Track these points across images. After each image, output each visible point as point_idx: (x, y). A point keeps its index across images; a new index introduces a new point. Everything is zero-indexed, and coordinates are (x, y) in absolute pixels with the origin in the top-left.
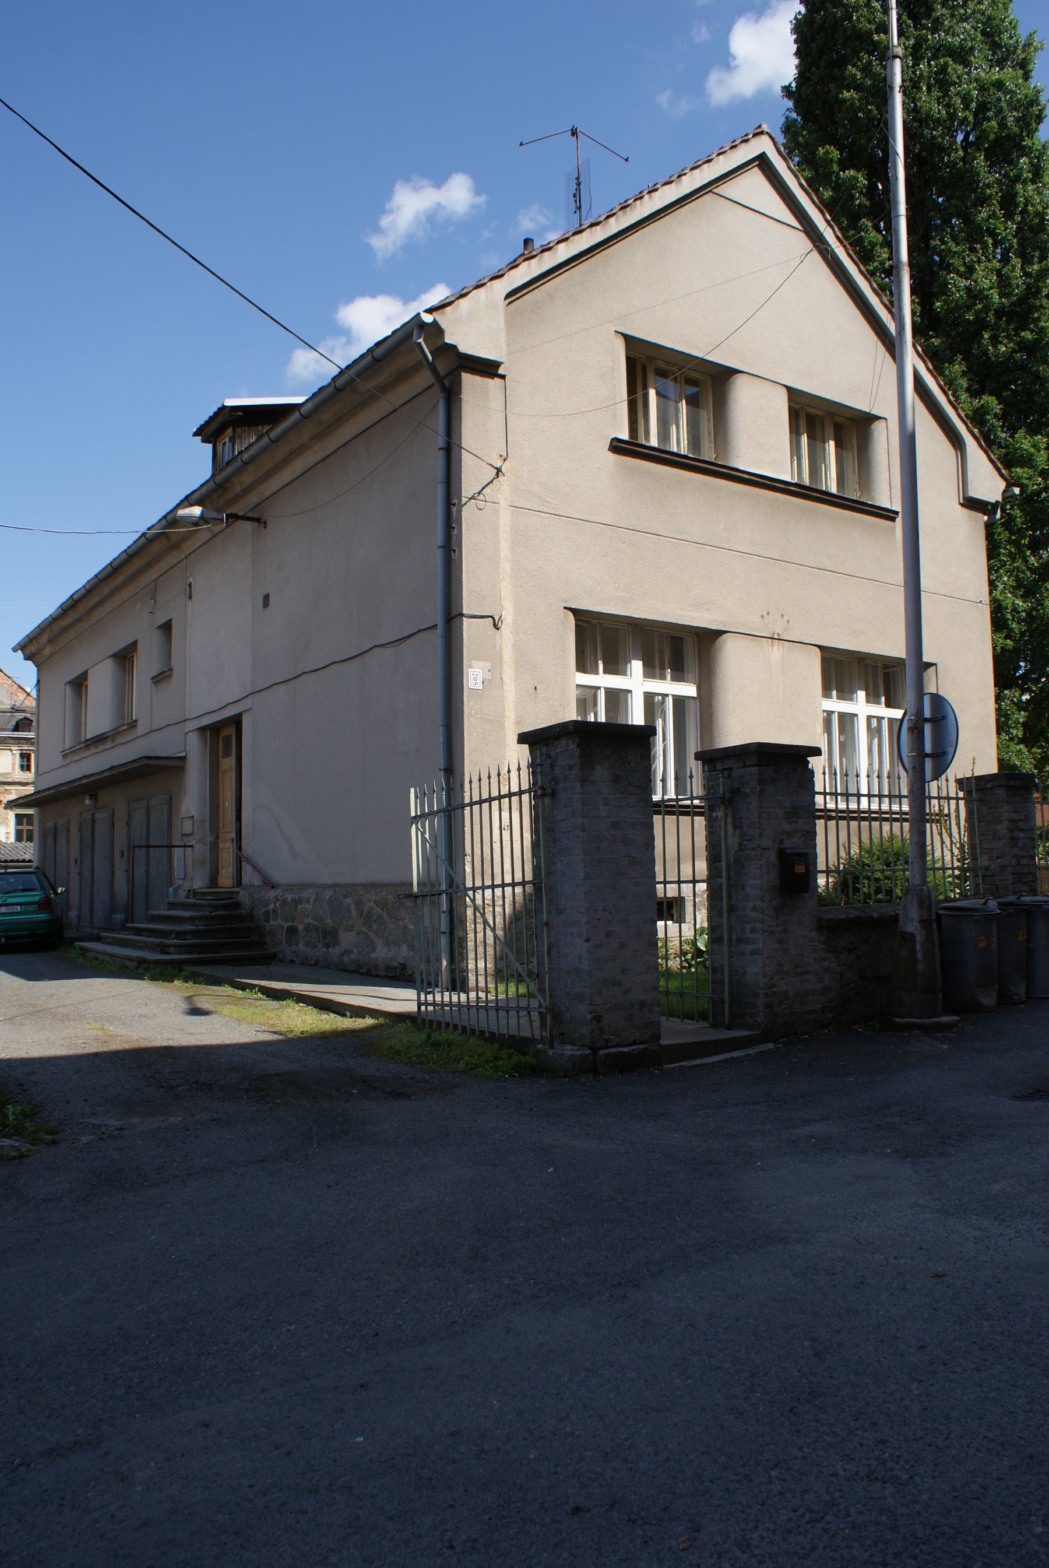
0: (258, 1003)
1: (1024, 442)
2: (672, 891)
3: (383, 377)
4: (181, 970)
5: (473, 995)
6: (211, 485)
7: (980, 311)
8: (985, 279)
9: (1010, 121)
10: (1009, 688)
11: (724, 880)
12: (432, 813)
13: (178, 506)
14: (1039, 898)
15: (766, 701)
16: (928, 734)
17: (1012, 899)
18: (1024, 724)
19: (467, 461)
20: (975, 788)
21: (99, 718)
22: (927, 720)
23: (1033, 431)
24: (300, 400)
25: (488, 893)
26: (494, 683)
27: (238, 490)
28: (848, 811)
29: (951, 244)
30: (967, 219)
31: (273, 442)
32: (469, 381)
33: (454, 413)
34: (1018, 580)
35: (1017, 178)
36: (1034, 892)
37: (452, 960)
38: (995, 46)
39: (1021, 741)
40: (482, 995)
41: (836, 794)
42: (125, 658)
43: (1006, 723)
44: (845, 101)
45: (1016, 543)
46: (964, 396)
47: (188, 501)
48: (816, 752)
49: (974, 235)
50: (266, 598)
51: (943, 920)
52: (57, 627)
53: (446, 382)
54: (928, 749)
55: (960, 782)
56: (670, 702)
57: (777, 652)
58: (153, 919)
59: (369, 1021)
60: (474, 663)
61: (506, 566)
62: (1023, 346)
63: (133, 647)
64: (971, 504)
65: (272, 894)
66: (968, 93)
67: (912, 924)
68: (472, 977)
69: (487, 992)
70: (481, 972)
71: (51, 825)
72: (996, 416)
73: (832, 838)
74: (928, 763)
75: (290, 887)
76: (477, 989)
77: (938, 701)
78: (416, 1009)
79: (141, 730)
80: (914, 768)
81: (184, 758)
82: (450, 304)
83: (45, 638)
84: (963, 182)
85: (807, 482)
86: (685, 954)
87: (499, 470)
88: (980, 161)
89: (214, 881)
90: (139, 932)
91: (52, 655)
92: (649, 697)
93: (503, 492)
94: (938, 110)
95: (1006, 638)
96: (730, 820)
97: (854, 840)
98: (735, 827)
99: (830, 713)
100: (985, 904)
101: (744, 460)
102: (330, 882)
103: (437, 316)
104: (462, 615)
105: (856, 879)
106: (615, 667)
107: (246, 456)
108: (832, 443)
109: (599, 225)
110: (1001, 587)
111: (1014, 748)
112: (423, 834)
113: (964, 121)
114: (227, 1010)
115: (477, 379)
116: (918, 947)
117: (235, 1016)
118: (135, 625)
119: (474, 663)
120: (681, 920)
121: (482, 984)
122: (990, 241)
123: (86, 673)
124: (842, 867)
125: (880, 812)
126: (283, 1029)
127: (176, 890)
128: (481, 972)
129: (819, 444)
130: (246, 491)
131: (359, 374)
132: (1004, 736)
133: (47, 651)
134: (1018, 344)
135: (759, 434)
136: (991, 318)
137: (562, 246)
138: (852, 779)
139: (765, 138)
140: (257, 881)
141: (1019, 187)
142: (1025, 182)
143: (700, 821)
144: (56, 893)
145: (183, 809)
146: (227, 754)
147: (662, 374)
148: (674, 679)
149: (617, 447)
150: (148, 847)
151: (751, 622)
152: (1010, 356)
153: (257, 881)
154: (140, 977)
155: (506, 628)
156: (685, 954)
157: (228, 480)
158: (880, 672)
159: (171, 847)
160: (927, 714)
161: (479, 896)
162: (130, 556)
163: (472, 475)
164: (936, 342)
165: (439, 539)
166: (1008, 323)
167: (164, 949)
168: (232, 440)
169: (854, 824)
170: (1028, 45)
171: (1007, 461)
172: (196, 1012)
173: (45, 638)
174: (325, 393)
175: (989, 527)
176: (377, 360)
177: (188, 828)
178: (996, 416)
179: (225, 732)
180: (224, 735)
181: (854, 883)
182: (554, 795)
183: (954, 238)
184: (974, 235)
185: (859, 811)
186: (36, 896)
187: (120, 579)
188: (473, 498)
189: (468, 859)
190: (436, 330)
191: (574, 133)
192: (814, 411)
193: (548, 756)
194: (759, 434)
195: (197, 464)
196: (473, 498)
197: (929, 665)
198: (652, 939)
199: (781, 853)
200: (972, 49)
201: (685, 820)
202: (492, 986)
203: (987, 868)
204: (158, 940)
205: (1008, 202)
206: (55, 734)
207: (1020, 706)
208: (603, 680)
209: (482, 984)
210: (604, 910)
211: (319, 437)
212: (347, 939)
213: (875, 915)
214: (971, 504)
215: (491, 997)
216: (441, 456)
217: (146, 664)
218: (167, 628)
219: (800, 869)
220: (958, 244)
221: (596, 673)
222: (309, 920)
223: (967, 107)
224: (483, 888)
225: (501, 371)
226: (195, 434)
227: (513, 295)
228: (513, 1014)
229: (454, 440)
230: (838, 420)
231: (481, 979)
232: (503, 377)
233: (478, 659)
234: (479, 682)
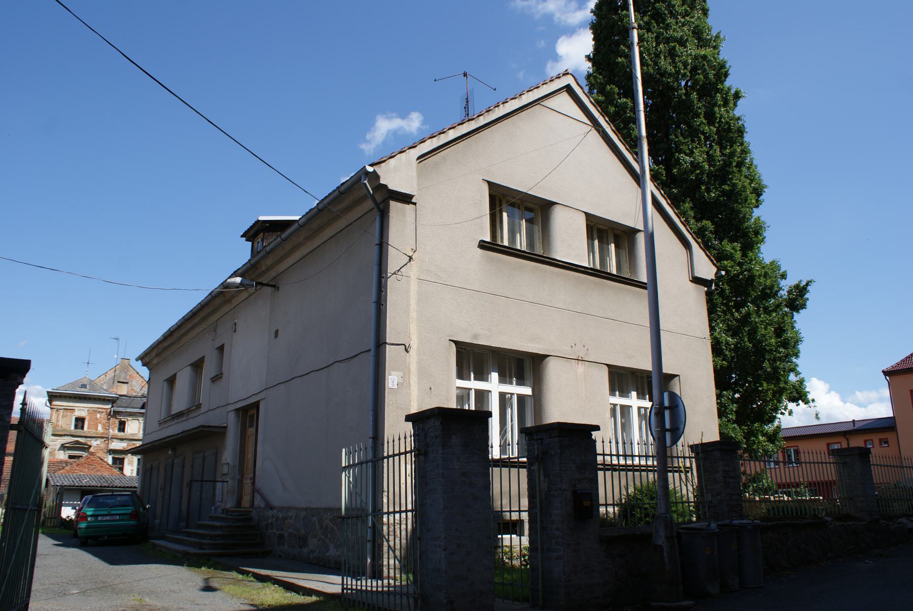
0: (249, 584)
1: (728, 247)
2: (515, 516)
3: (345, 204)
4: (209, 560)
5: (386, 581)
6: (248, 265)
7: (698, 174)
8: (700, 157)
9: (711, 76)
10: (726, 390)
11: (538, 510)
12: (354, 465)
13: (230, 277)
14: (745, 521)
15: (575, 396)
16: (668, 419)
17: (727, 522)
18: (736, 412)
19: (392, 253)
20: (701, 451)
21: (180, 403)
22: (666, 408)
23: (732, 241)
24: (297, 218)
25: (397, 516)
26: (404, 384)
27: (264, 268)
28: (626, 465)
29: (681, 138)
30: (689, 125)
31: (283, 240)
32: (393, 204)
33: (385, 224)
34: (728, 326)
35: (715, 104)
36: (742, 517)
37: (373, 559)
38: (699, 39)
39: (735, 422)
40: (392, 582)
41: (611, 455)
42: (198, 366)
43: (725, 411)
44: (619, 63)
45: (726, 305)
46: (692, 221)
47: (235, 274)
48: (597, 428)
49: (693, 133)
50: (277, 332)
51: (682, 536)
52: (161, 347)
53: (381, 206)
54: (668, 426)
55: (693, 448)
56: (515, 398)
57: (581, 368)
58: (199, 526)
59: (314, 598)
60: (392, 372)
61: (414, 314)
62: (724, 193)
63: (202, 360)
64: (697, 280)
65: (270, 513)
66: (686, 61)
67: (661, 540)
68: (385, 570)
69: (395, 579)
70: (392, 566)
71: (149, 466)
72: (711, 232)
73: (616, 482)
74: (668, 436)
75: (282, 509)
76: (389, 578)
77: (674, 397)
78: (340, 591)
79: (203, 410)
80: (659, 438)
81: (226, 427)
82: (384, 161)
83: (154, 353)
84: (686, 107)
85: (598, 267)
86: (524, 556)
87: (411, 258)
88: (694, 95)
89: (239, 503)
90: (189, 534)
91: (158, 363)
92: (502, 396)
93: (413, 270)
94: (670, 69)
95: (723, 360)
96: (542, 472)
97: (631, 483)
98: (545, 476)
99: (615, 405)
100: (709, 525)
101: (560, 253)
102: (305, 506)
103: (376, 168)
104: (386, 343)
105: (633, 508)
106: (481, 376)
107: (268, 249)
108: (613, 245)
109: (471, 120)
110: (718, 330)
111: (731, 426)
112: (349, 477)
113: (684, 75)
114: (227, 588)
115: (399, 205)
116: (665, 554)
117: (232, 592)
118: (204, 348)
119: (392, 372)
120: (521, 534)
121: (392, 574)
122: (702, 137)
123: (175, 375)
124: (623, 501)
125: (647, 466)
126: (258, 603)
127: (216, 508)
128: (392, 566)
129: (605, 246)
130: (269, 269)
131: (329, 204)
132: (724, 419)
133: (155, 361)
134: (721, 192)
135: (569, 240)
136: (705, 177)
137: (451, 131)
138: (628, 446)
139: (570, 77)
140: (262, 505)
141: (716, 109)
142: (719, 106)
143: (524, 472)
144: (144, 508)
145: (223, 458)
146: (251, 426)
147: (513, 205)
148: (518, 384)
149: (483, 245)
150: (202, 481)
151: (566, 351)
152: (717, 199)
153: (262, 505)
154: (182, 565)
155: (412, 352)
156: (524, 556)
157: (257, 263)
158: (645, 381)
159: (215, 481)
160: (666, 404)
161: (391, 518)
162: (202, 307)
163: (394, 260)
164: (675, 191)
165: (373, 298)
166: (715, 181)
167: (201, 546)
168: (263, 241)
169: (630, 474)
170: (717, 37)
171: (718, 258)
172: (208, 588)
173: (154, 353)
174: (312, 213)
175: (709, 294)
176: (341, 193)
177: (225, 470)
178: (711, 232)
179: (250, 413)
180: (249, 414)
181: (631, 511)
182: (426, 454)
183: (682, 135)
184: (693, 133)
185: (633, 465)
186: (129, 510)
187: (196, 320)
188: (395, 273)
189: (385, 494)
190: (375, 176)
191: (465, 75)
192: (602, 227)
193: (423, 429)
194: (569, 240)
195: (243, 253)
196: (395, 273)
197: (673, 376)
198: (496, 545)
199: (575, 493)
200: (687, 40)
201: (514, 471)
202: (398, 576)
203: (711, 502)
204: (197, 540)
205: (710, 118)
206: (157, 411)
207: (733, 400)
208: (473, 384)
209: (392, 574)
210: (456, 530)
211: (309, 238)
212: (313, 543)
213: (637, 533)
214: (697, 280)
215: (398, 584)
216: (376, 248)
217: (209, 370)
218: (221, 349)
219: (587, 503)
220: (685, 138)
221: (469, 379)
222: (291, 530)
223: (685, 68)
224: (394, 512)
225: (413, 200)
226: (242, 236)
227: (422, 158)
228: (398, 597)
229: (384, 240)
230: (617, 232)
231: (392, 571)
232: (415, 204)
233: (394, 370)
234: (396, 384)
